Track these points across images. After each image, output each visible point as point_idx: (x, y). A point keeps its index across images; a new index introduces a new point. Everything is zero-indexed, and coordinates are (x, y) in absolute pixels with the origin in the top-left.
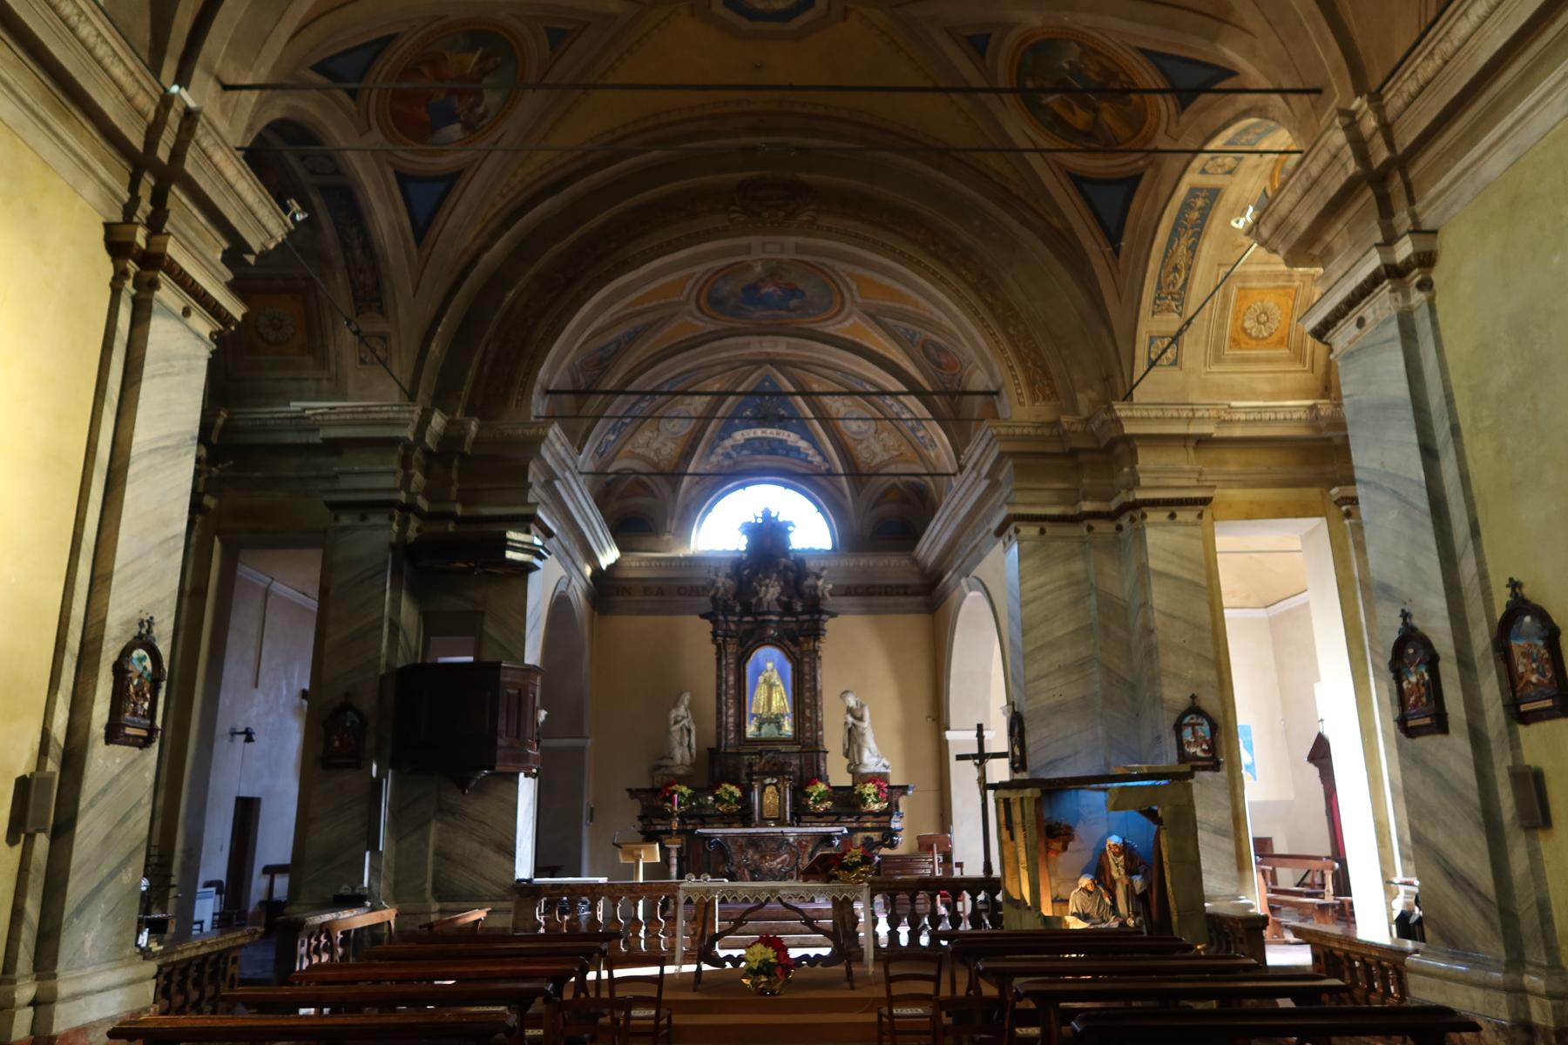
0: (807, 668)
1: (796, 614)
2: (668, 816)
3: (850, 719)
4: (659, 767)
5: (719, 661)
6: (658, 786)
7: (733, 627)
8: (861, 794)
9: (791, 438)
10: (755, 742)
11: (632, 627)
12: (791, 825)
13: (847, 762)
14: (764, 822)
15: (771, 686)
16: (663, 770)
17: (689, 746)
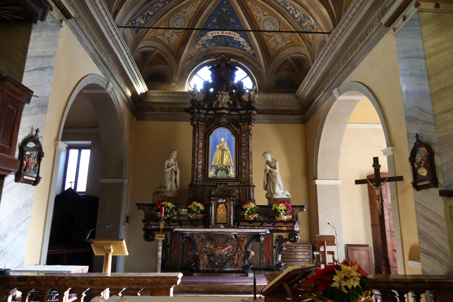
0: (244, 140)
1: (238, 110)
2: (158, 220)
3: (269, 168)
4: (158, 192)
5: (194, 134)
6: (155, 202)
7: (202, 116)
8: (276, 210)
9: (236, 36)
10: (213, 179)
11: (154, 127)
12: (234, 228)
13: (266, 192)
14: (217, 225)
15: (223, 150)
16: (160, 194)
17: (175, 181)
